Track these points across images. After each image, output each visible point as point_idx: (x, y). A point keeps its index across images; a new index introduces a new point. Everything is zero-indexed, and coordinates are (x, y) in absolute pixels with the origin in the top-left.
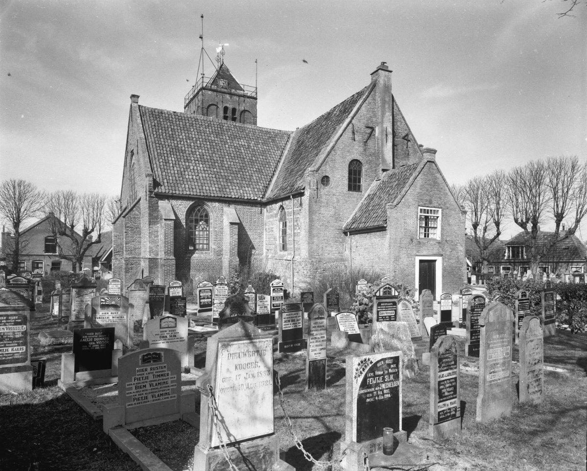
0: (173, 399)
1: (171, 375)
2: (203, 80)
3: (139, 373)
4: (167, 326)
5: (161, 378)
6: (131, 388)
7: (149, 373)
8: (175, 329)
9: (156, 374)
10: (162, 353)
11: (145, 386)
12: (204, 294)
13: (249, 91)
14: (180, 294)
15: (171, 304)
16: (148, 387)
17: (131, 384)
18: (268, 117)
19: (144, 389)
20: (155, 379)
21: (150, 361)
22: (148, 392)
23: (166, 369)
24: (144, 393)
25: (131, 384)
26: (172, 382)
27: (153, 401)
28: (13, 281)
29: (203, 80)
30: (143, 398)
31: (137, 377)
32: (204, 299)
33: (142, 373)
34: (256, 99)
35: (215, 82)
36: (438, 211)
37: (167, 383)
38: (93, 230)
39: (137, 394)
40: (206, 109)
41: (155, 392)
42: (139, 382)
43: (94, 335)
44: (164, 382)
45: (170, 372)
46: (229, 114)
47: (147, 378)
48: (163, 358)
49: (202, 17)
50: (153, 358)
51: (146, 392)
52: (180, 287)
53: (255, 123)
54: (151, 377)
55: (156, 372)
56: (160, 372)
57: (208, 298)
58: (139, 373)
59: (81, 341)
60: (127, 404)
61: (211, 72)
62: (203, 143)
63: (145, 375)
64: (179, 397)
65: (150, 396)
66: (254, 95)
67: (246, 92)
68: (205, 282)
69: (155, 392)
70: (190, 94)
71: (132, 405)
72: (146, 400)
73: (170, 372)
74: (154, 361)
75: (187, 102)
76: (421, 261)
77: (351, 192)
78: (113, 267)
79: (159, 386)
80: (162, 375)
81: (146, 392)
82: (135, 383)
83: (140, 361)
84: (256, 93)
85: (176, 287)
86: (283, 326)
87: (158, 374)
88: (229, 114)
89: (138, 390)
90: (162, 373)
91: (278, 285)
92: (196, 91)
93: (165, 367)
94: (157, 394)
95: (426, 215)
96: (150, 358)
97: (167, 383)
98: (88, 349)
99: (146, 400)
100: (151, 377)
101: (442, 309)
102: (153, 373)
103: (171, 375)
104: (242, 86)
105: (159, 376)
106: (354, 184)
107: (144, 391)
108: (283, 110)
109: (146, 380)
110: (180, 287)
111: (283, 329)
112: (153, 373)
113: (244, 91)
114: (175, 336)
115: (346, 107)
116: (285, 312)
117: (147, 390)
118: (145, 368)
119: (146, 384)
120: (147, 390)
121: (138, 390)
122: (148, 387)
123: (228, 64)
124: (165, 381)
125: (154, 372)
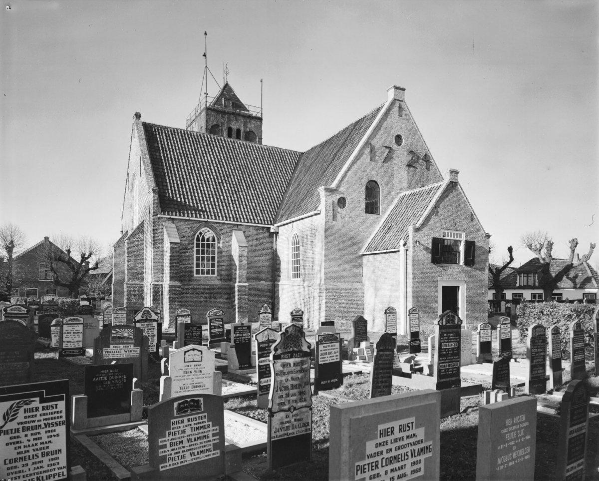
0: (215, 456)
1: (213, 426)
2: (206, 100)
3: (174, 426)
4: (192, 360)
5: (200, 431)
6: (165, 446)
7: (186, 426)
8: (200, 363)
9: (196, 426)
10: (201, 399)
11: (181, 442)
12: (216, 324)
13: (254, 112)
14: (189, 322)
15: (185, 334)
16: (186, 444)
17: (165, 441)
18: (273, 136)
19: (181, 445)
20: (194, 432)
21: (188, 411)
22: (185, 449)
23: (206, 420)
24: (181, 451)
25: (165, 441)
26: (214, 435)
27: (192, 460)
28: (79, 320)
29: (206, 100)
30: (180, 458)
31: (172, 431)
32: (215, 328)
33: (178, 425)
34: (260, 119)
35: (218, 100)
36: (461, 235)
37: (208, 437)
38: (90, 255)
39: (173, 452)
40: (213, 129)
41: (195, 449)
42: (174, 437)
43: (109, 371)
44: (205, 436)
45: (210, 423)
46: (234, 134)
47: (184, 432)
48: (202, 406)
49: (206, 34)
50: (191, 406)
51: (183, 449)
52: (188, 315)
53: (260, 142)
54: (188, 431)
55: (195, 424)
56: (198, 423)
57: (219, 328)
58: (174, 426)
59: (94, 379)
60: (161, 466)
61: (214, 92)
62: (209, 164)
63: (182, 429)
64: (222, 453)
65: (188, 454)
66: (259, 115)
67: (251, 113)
68: (216, 310)
69: (195, 449)
70: (192, 115)
71: (166, 466)
72: (183, 460)
73: (210, 423)
74: (192, 410)
75: (189, 123)
76: (444, 287)
77: (367, 214)
78: (92, 419)
79: (198, 442)
80: (202, 427)
81: (183, 449)
82: (170, 438)
83: (175, 411)
84: (262, 114)
85: (184, 316)
86: (320, 360)
87: (197, 426)
88: (234, 134)
89: (173, 447)
90: (202, 425)
91: (298, 314)
92: (199, 112)
93: (205, 416)
94: (196, 451)
95: (455, 239)
96: (187, 407)
97: (208, 437)
98: (102, 389)
99: (183, 460)
100: (188, 431)
101: (481, 341)
102: (191, 425)
103: (213, 426)
104: (247, 107)
105: (198, 428)
106: (372, 208)
107: (180, 448)
108: (291, 128)
109: (183, 435)
110: (188, 315)
111: (320, 363)
112: (191, 425)
113: (248, 111)
114: (201, 371)
115: (357, 127)
116: (322, 344)
117: (184, 447)
118: (181, 419)
119: (183, 439)
120: (184, 447)
121: (173, 447)
122: (186, 444)
123: (231, 84)
124: (206, 434)
125: (192, 423)
